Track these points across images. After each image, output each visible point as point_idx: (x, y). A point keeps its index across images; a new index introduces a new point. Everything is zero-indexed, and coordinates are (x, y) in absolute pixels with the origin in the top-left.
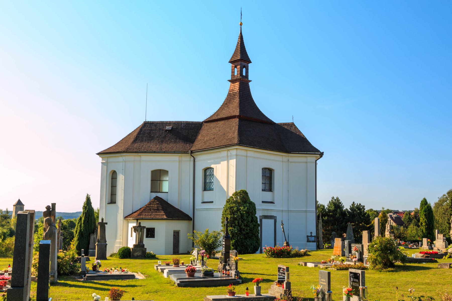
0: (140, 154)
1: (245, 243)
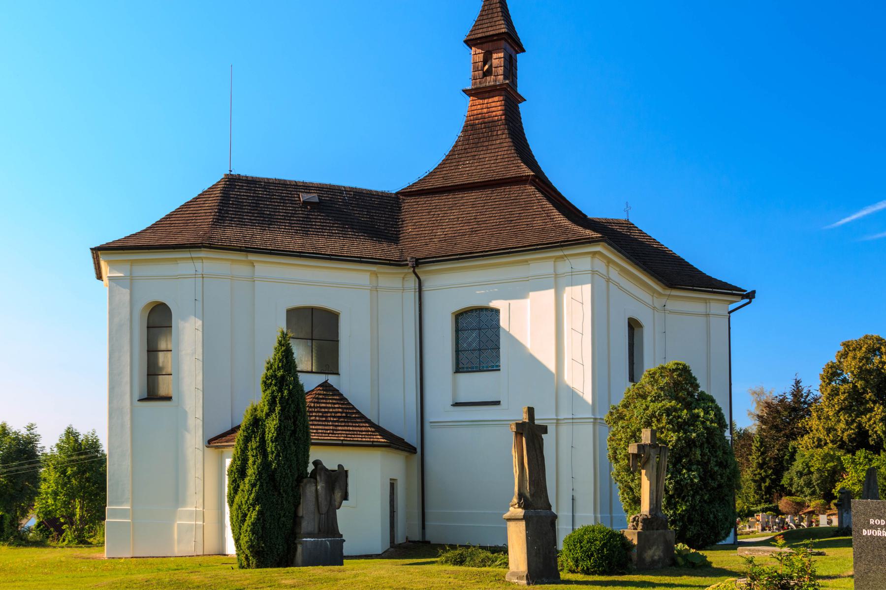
0: (252, 257)
1: (711, 516)
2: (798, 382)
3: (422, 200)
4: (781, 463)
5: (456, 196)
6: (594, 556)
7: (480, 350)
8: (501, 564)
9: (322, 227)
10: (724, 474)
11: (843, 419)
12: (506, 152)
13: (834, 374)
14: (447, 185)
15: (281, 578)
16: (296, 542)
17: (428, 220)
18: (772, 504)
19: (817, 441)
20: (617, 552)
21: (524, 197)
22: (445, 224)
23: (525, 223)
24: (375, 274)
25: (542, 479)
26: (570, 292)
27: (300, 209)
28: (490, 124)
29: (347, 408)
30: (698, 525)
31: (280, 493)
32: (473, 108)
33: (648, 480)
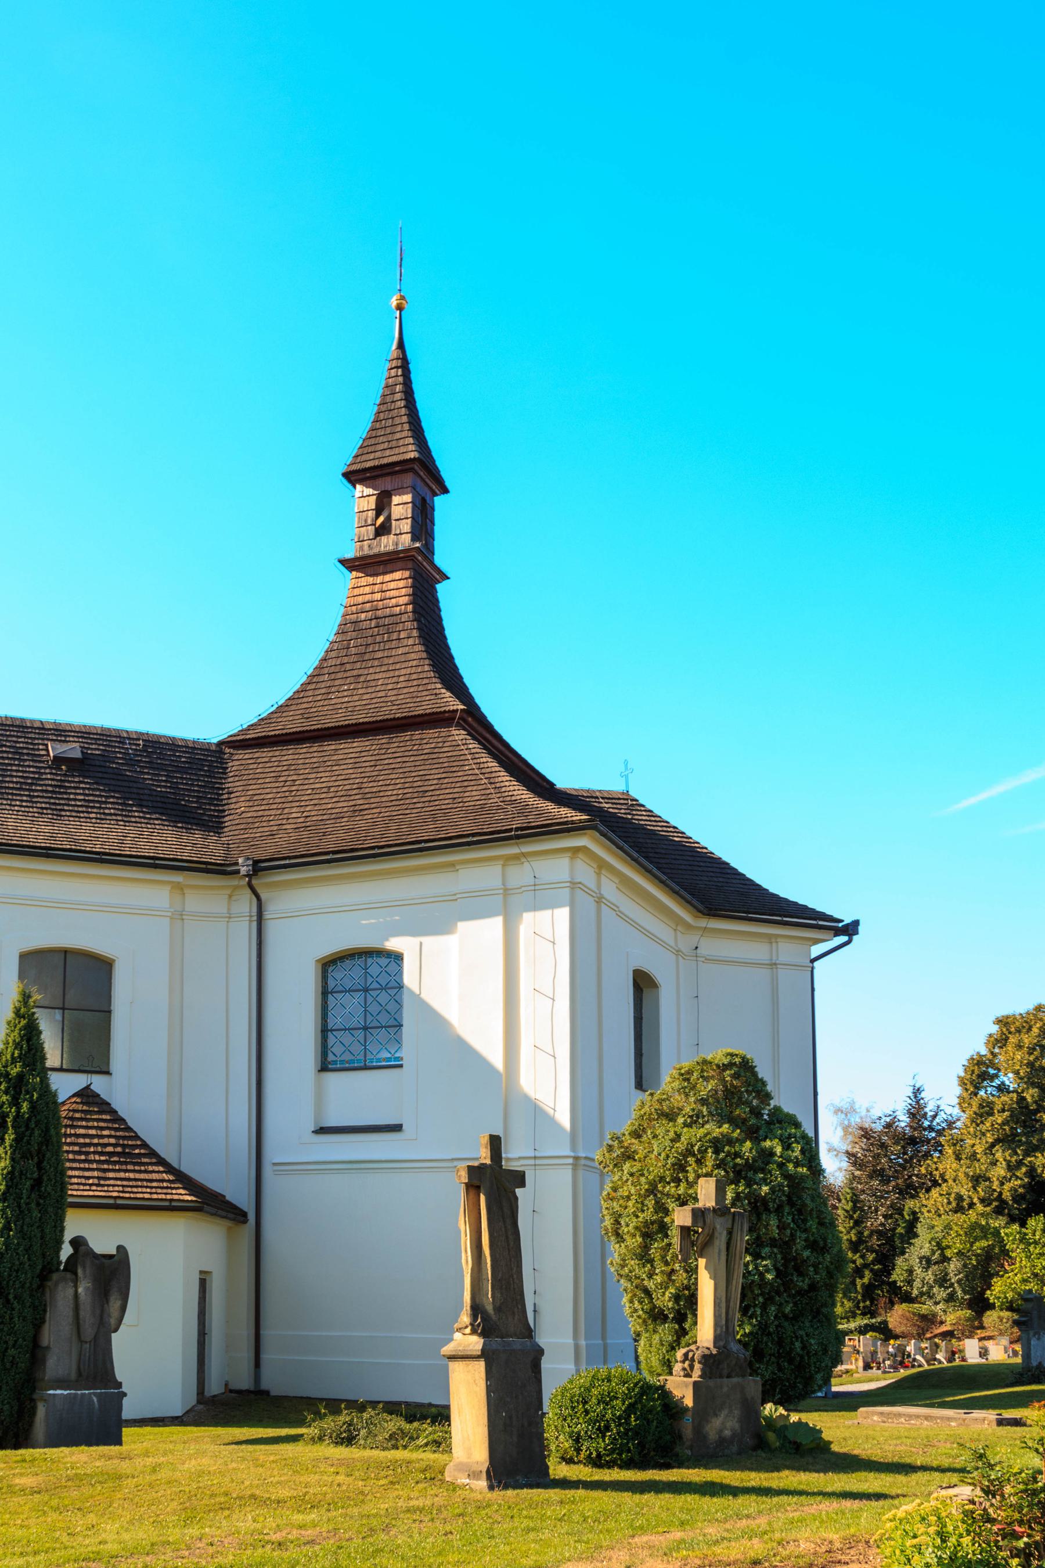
1: (798, 1344)
2: (917, 1091)
3: (264, 755)
4: (890, 1241)
5: (325, 748)
6: (612, 1430)
7: (365, 1028)
8: (426, 1445)
9: (87, 804)
10: (819, 1263)
11: (1001, 1160)
12: (413, 670)
13: (984, 1076)
14: (308, 728)
15: (12, 1472)
16: (35, 1396)
17: (275, 790)
18: (875, 1317)
19: (955, 1199)
20: (655, 1423)
21: (446, 749)
22: (306, 798)
23: (451, 796)
24: (179, 888)
25: (515, 1276)
26: (531, 923)
27: (48, 771)
28: (387, 619)
29: (124, 1138)
30: (773, 1363)
31: (8, 1301)
32: (356, 592)
33: (710, 1278)
